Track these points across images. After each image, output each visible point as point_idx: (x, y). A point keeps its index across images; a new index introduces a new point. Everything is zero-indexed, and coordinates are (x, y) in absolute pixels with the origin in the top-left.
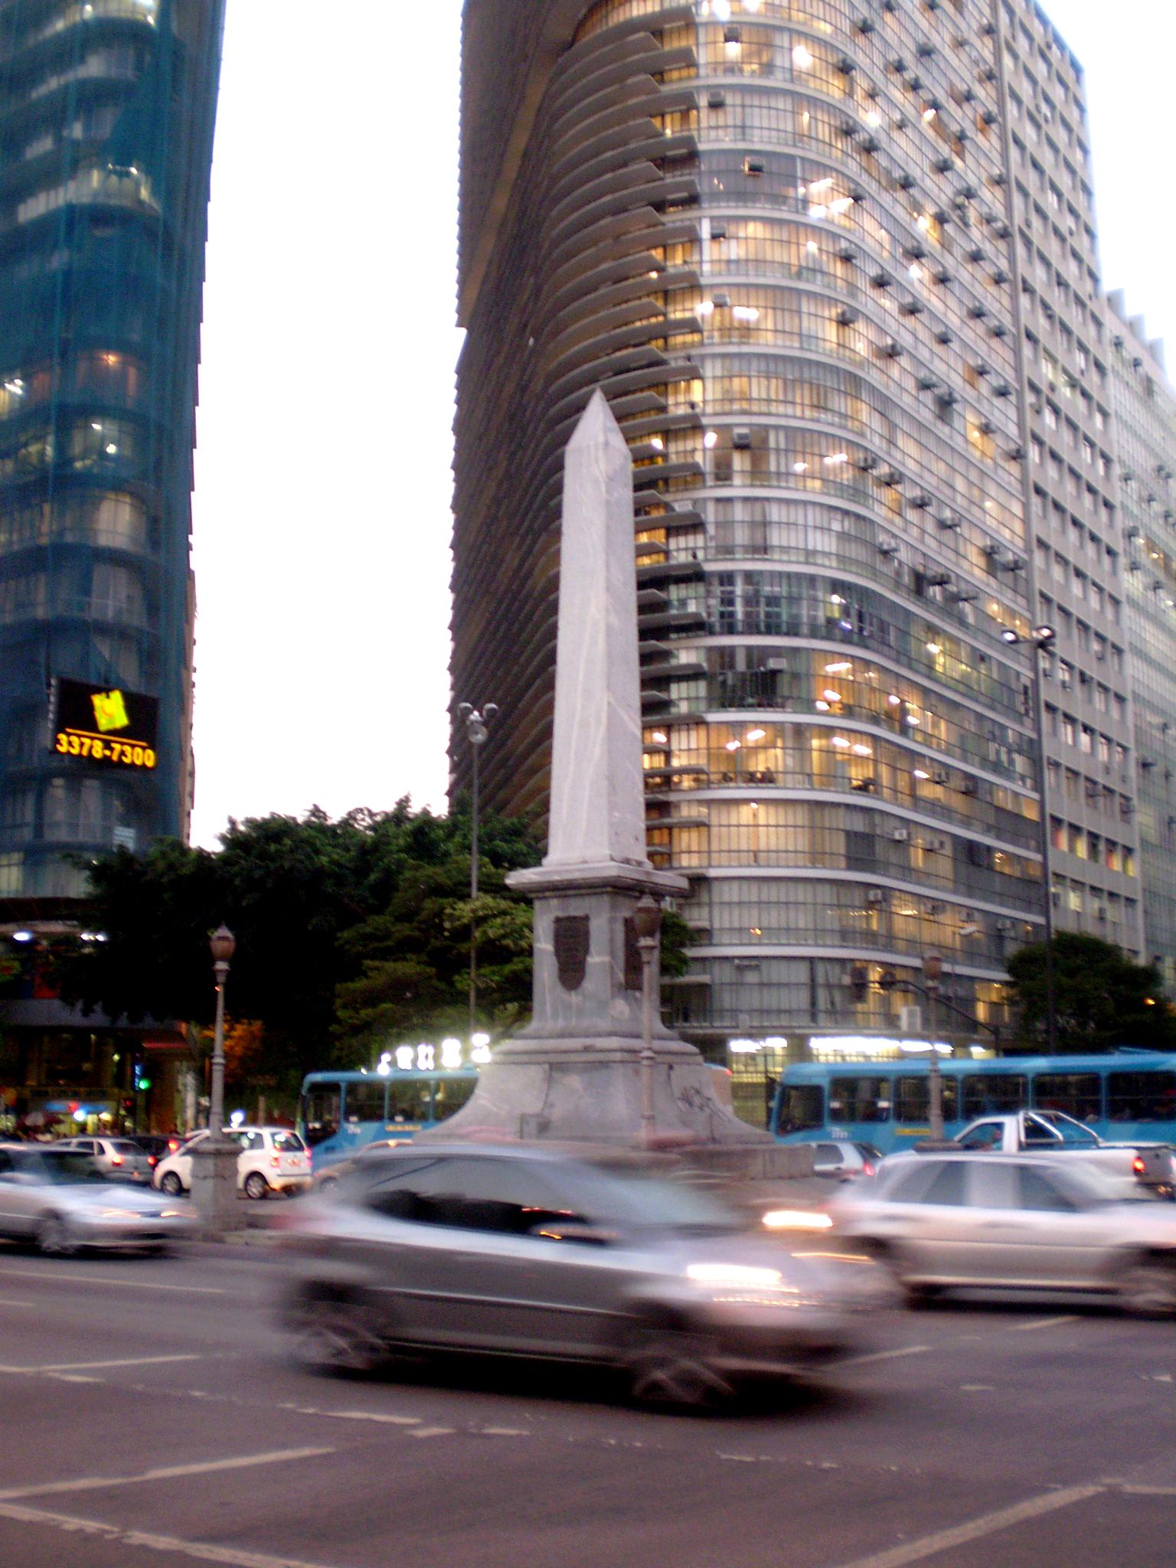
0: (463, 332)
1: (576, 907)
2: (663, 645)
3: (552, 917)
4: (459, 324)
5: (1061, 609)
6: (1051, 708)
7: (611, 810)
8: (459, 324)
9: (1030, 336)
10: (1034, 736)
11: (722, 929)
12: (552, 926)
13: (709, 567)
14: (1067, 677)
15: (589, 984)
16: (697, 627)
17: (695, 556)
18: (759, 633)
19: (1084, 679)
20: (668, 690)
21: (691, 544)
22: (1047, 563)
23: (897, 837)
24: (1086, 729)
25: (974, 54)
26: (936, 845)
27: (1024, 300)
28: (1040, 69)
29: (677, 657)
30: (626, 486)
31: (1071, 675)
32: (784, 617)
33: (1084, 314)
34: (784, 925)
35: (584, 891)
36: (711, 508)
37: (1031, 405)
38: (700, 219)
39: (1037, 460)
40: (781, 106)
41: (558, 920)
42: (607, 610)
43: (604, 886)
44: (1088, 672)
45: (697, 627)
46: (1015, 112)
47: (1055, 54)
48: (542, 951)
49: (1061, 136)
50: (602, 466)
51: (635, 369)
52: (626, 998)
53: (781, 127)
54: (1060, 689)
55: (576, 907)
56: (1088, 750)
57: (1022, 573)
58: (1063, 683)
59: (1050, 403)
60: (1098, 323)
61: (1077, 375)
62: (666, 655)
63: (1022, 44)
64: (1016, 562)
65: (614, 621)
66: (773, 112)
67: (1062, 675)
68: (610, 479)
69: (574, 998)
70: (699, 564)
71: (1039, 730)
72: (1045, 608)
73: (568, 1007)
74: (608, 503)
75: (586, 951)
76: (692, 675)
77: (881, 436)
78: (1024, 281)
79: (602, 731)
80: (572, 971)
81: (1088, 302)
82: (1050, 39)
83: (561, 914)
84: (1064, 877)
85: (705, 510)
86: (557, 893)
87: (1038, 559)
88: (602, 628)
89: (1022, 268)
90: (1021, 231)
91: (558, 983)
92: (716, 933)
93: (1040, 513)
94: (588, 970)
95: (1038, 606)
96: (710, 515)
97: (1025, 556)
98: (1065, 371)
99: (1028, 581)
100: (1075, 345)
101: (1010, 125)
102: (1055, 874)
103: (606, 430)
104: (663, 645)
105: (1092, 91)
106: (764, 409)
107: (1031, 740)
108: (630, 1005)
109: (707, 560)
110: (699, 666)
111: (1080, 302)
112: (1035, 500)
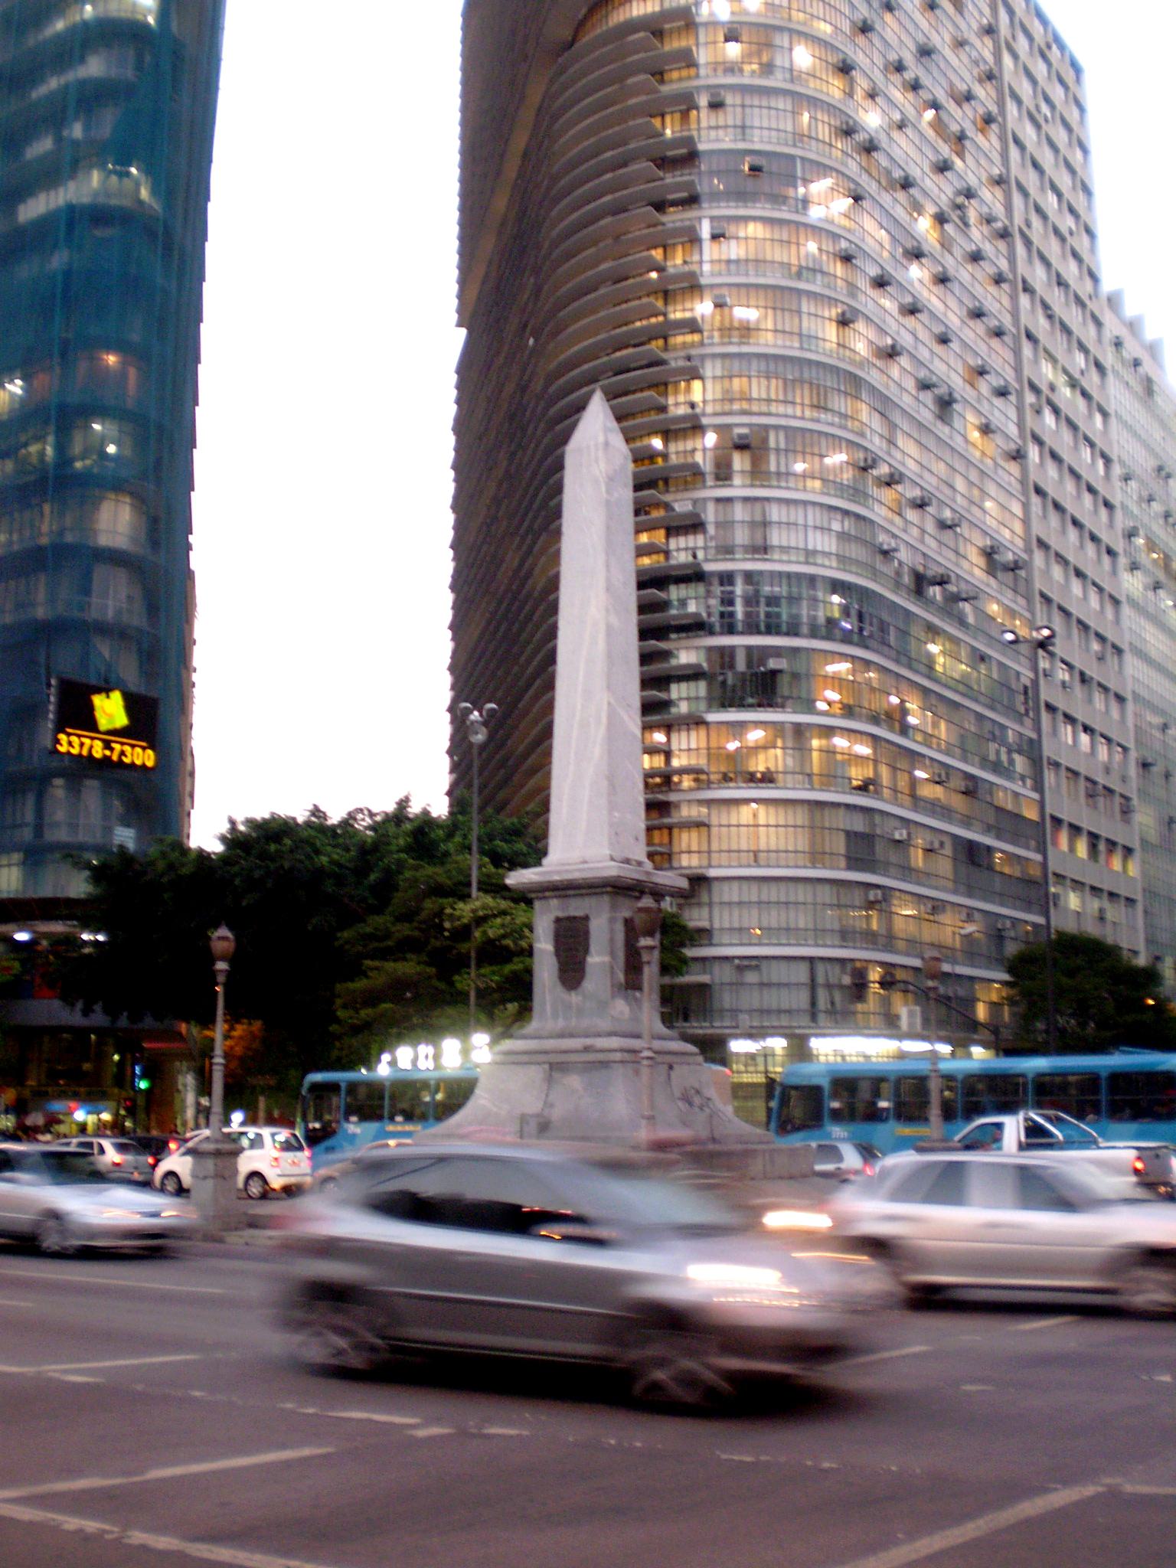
0: (463, 332)
1: (576, 907)
2: (663, 645)
3: (552, 917)
4: (459, 324)
5: (1061, 609)
6: (1051, 708)
7: (611, 810)
8: (459, 324)
9: (1030, 336)
10: (1034, 736)
11: (722, 929)
12: (552, 926)
13: (709, 567)
14: (1067, 677)
15: (589, 984)
16: (697, 627)
17: (695, 556)
18: (759, 633)
19: (1084, 679)
20: (668, 690)
21: (691, 544)
22: (1047, 563)
23: (897, 837)
24: (1086, 729)
25: (974, 54)
26: (936, 845)
27: (1024, 300)
28: (1040, 69)
29: (677, 657)
30: (626, 486)
31: (1071, 675)
32: (784, 617)
33: (1084, 314)
34: (784, 925)
35: (584, 891)
36: (711, 508)
37: (1031, 405)
38: (700, 219)
39: (1037, 460)
40: (781, 106)
41: (558, 920)
42: (607, 610)
43: (604, 886)
44: (1088, 672)
45: (697, 627)
46: (1015, 112)
47: (1055, 54)
48: (542, 951)
49: (1061, 136)
50: (602, 466)
51: (635, 369)
52: (626, 998)
53: (781, 127)
54: (1060, 689)
55: (576, 907)
56: (1088, 750)
57: (1022, 573)
58: (1063, 683)
59: (1050, 403)
60: (1098, 323)
61: (1077, 375)
62: (666, 655)
63: (1022, 44)
64: (1016, 562)
65: (614, 621)
66: (773, 112)
67: (1062, 675)
68: (610, 479)
69: (574, 998)
70: (699, 564)
71: (1039, 730)
72: (1045, 608)
73: (568, 1007)
74: (608, 503)
75: (586, 951)
76: (692, 675)
77: (881, 436)
78: (1024, 281)
79: (602, 731)
80: (572, 971)
81: (1088, 302)
82: (1050, 39)
83: (561, 914)
84: (1064, 877)
85: (705, 510)
86: (557, 893)
87: (1038, 559)
88: (602, 628)
89: (1022, 268)
90: (1021, 231)
91: (558, 983)
92: (716, 933)
93: (1040, 513)
94: (588, 970)
95: (1038, 606)
96: (710, 515)
97: (1025, 556)
98: (1065, 371)
99: (1028, 581)
100: (1075, 345)
101: (1010, 125)
102: (1055, 874)
103: (606, 430)
104: (663, 645)
105: (1092, 91)
106: (764, 409)
107: (1031, 740)
108: (630, 1005)
109: (707, 560)
110: (699, 666)
111: (1080, 302)
112: (1035, 500)
